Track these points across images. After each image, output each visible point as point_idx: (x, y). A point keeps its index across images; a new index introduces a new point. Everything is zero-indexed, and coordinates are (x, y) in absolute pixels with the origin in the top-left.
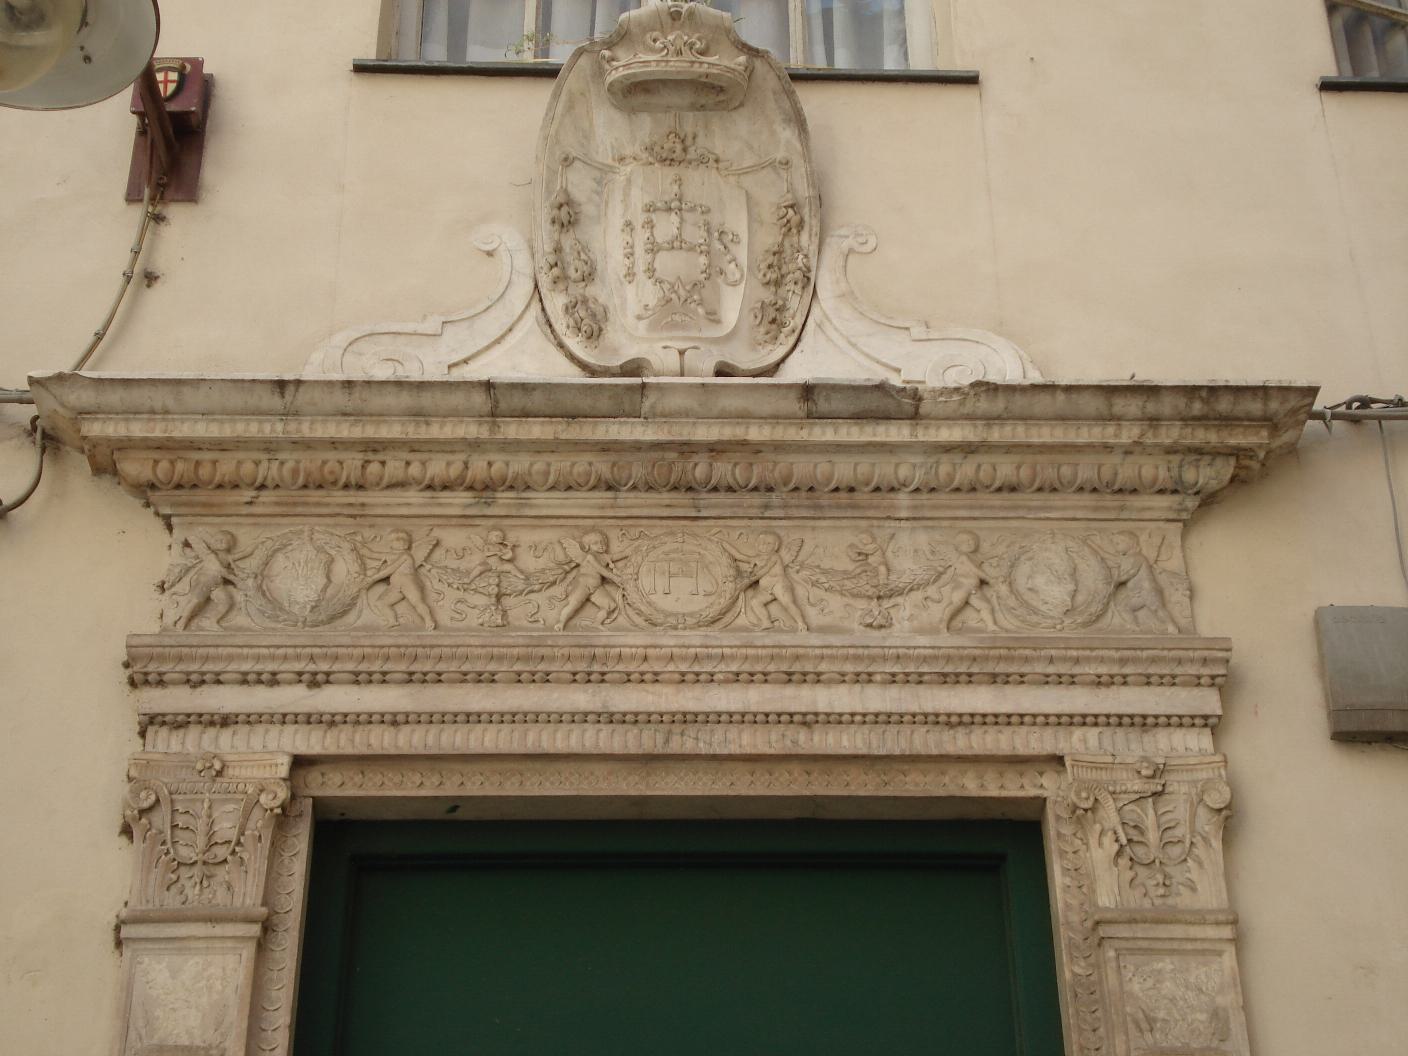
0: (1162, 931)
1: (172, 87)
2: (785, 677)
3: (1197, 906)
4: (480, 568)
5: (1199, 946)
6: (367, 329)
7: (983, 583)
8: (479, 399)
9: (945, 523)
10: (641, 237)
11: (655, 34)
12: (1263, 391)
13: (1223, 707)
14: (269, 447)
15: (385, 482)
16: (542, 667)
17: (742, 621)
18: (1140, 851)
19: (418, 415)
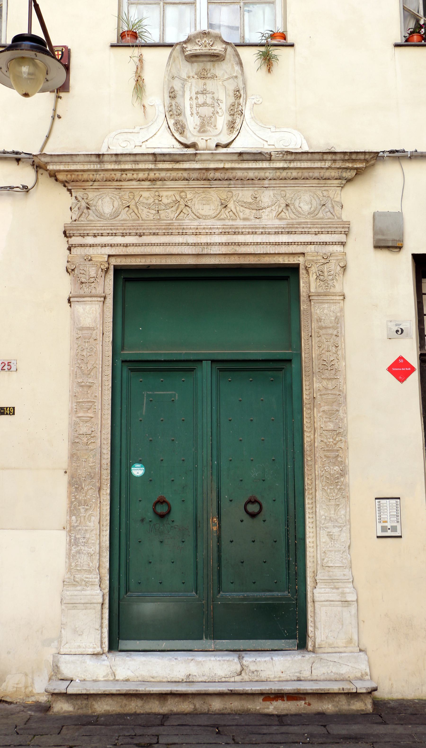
0: (325, 298)
1: (60, 56)
2: (234, 233)
3: (335, 291)
4: (153, 203)
5: (334, 301)
6: (120, 131)
7: (287, 205)
8: (151, 158)
9: (277, 188)
10: (195, 101)
11: (199, 39)
12: (365, 153)
13: (347, 240)
14: (96, 171)
15: (127, 180)
16: (170, 231)
17: (222, 217)
18: (322, 277)
19: (135, 162)
